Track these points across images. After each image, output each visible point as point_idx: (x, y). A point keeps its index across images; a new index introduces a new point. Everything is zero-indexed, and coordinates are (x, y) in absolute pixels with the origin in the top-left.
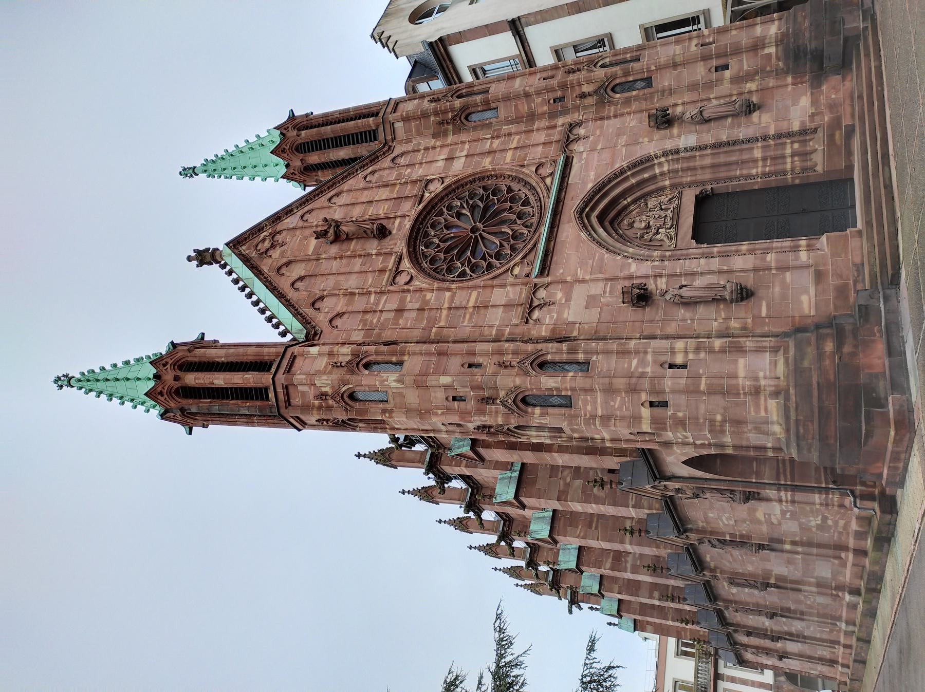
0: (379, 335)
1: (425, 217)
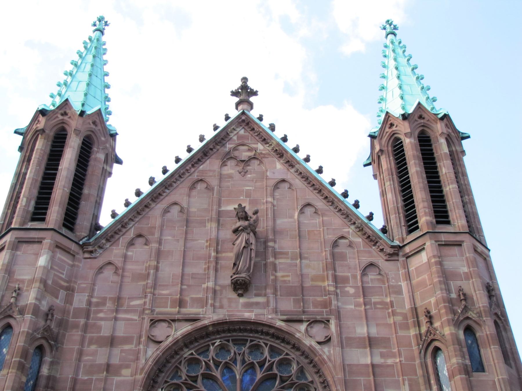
1: (267, 334)
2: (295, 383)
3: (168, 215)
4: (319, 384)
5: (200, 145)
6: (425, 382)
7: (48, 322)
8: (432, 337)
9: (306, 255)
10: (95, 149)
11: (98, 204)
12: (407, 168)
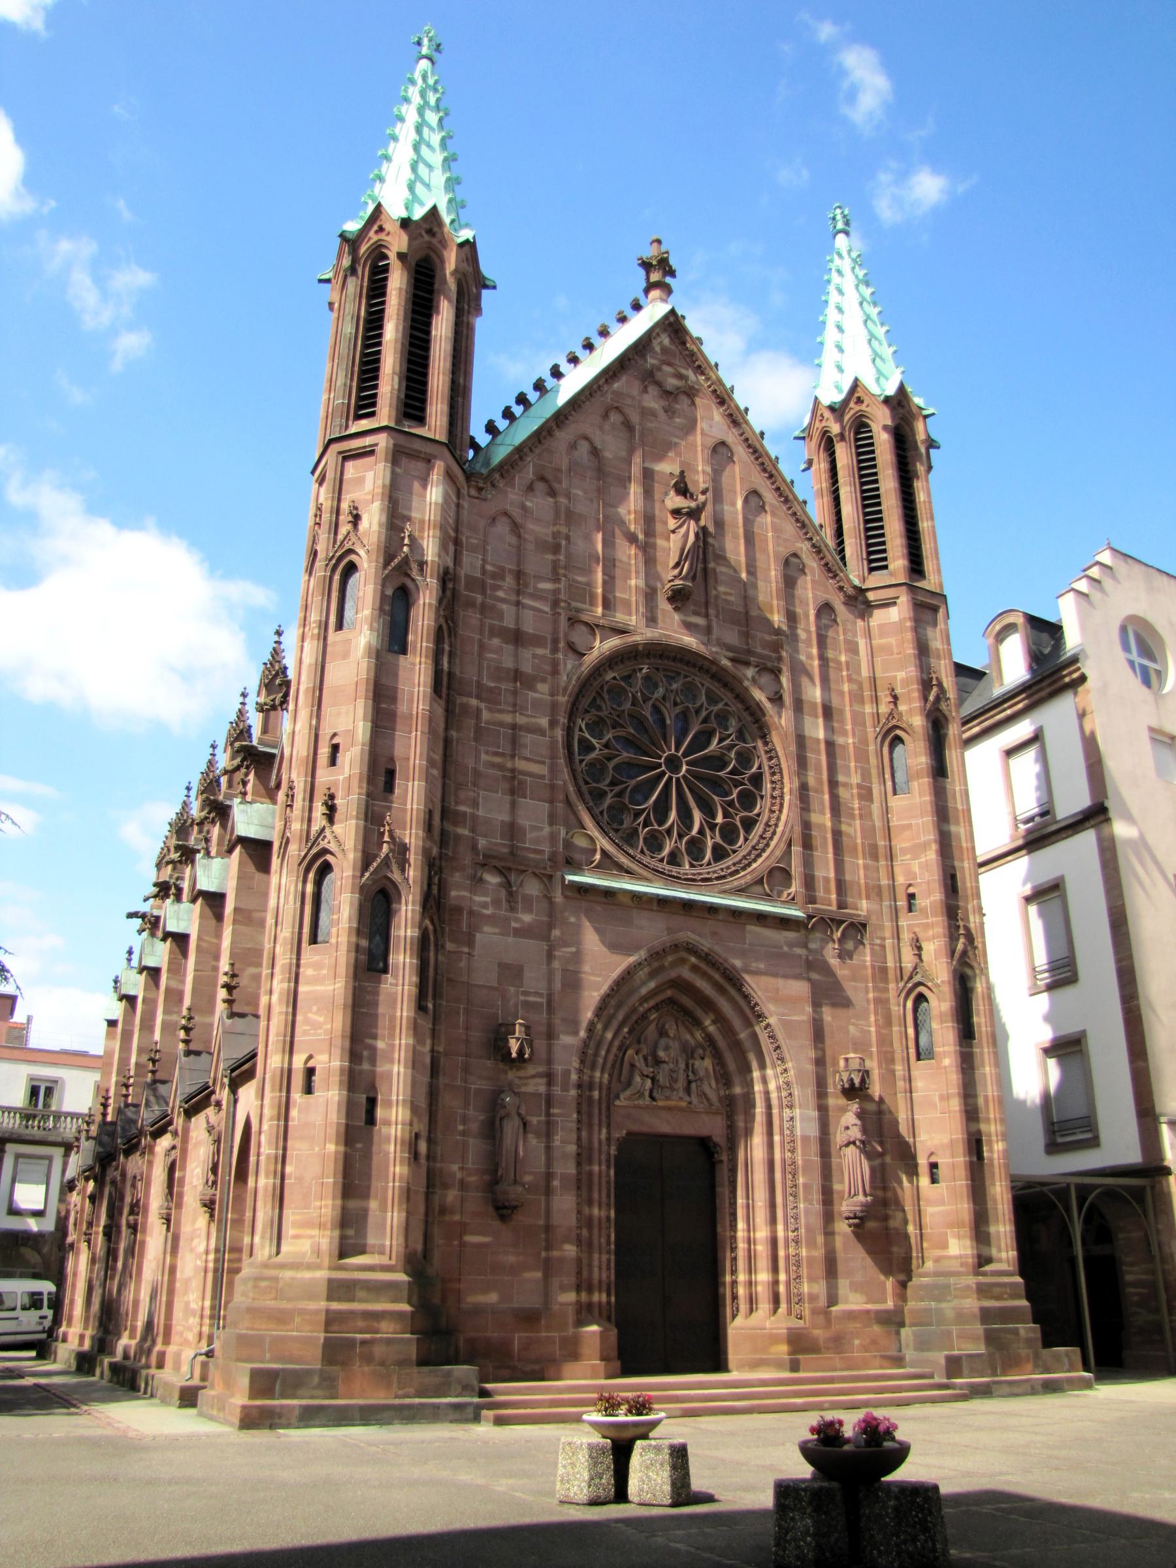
0: (471, 604)
3: (576, 454)
4: (763, 753)
8: (894, 722)
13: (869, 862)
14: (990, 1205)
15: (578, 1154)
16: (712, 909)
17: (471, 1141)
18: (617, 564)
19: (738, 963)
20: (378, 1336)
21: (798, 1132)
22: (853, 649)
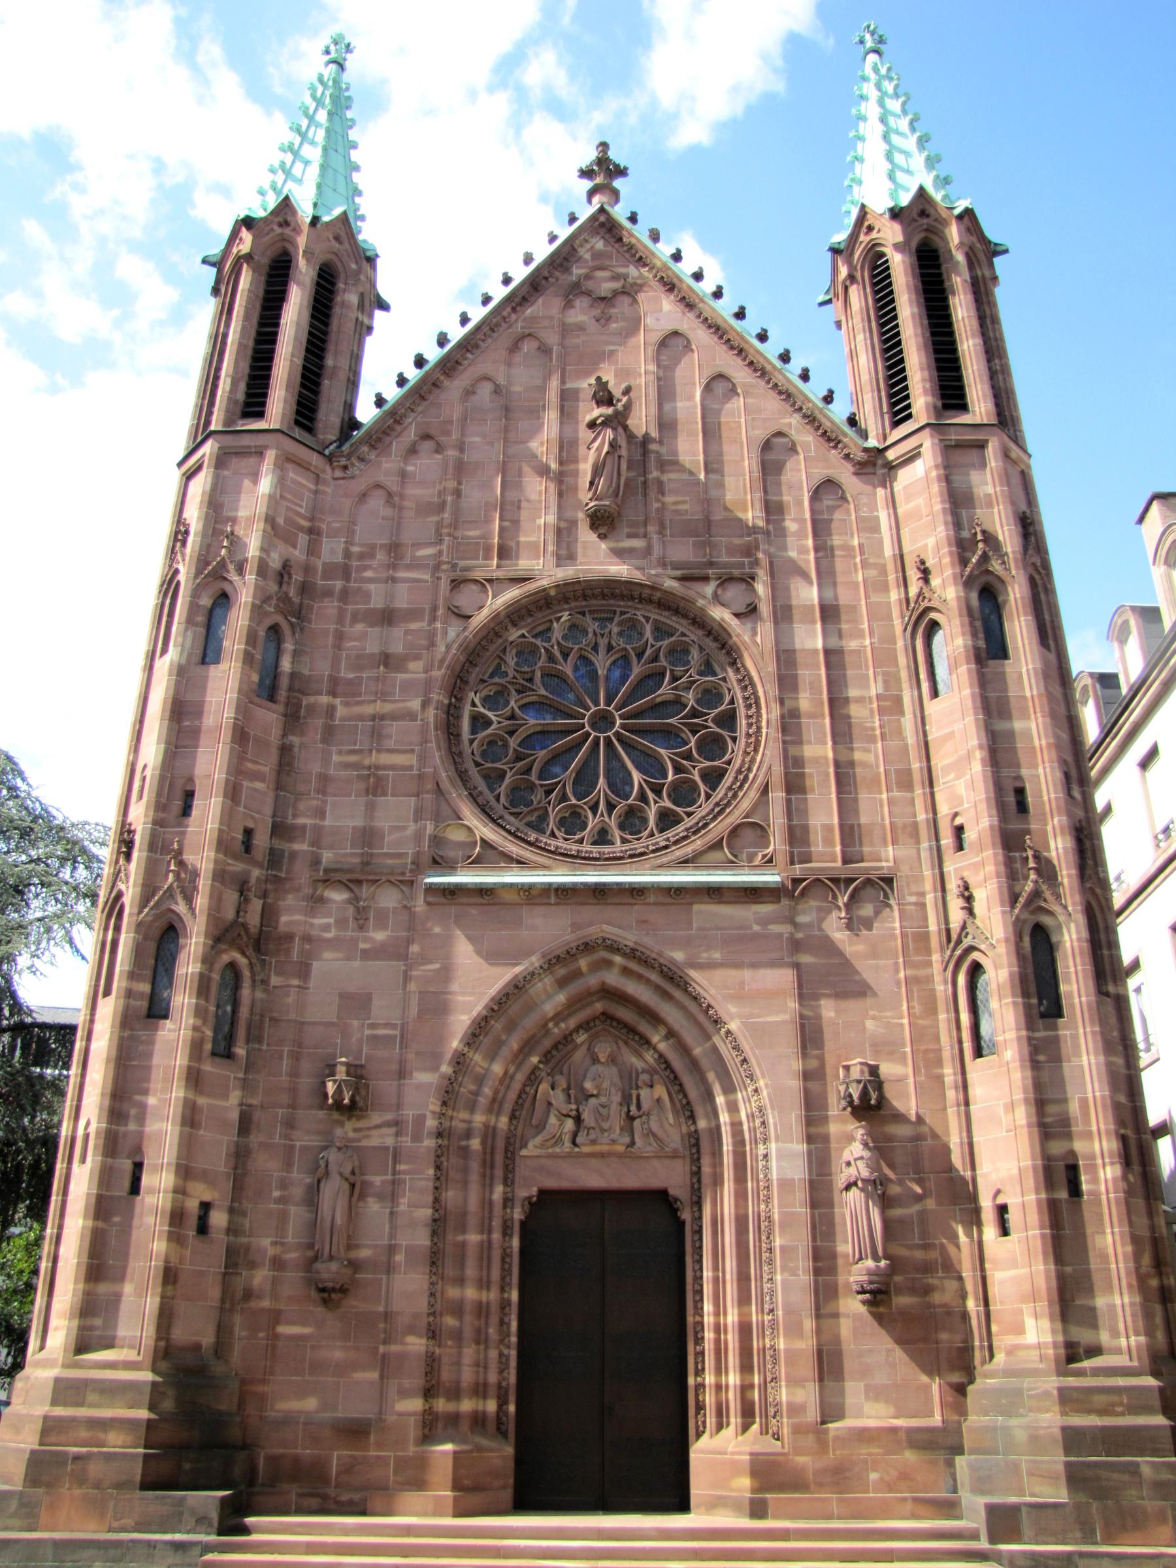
2: (695, 681)
3: (475, 399)
4: (735, 683)
5: (526, 271)
6: (910, 676)
7: (285, 587)
9: (715, 466)
10: (341, 285)
11: (353, 384)
12: (894, 309)
13: (896, 794)
14: (1094, 1265)
15: (435, 1220)
16: (636, 892)
17: (293, 1209)
18: (523, 504)
19: (679, 956)
20: (105, 1449)
21: (774, 1175)
22: (872, 526)
